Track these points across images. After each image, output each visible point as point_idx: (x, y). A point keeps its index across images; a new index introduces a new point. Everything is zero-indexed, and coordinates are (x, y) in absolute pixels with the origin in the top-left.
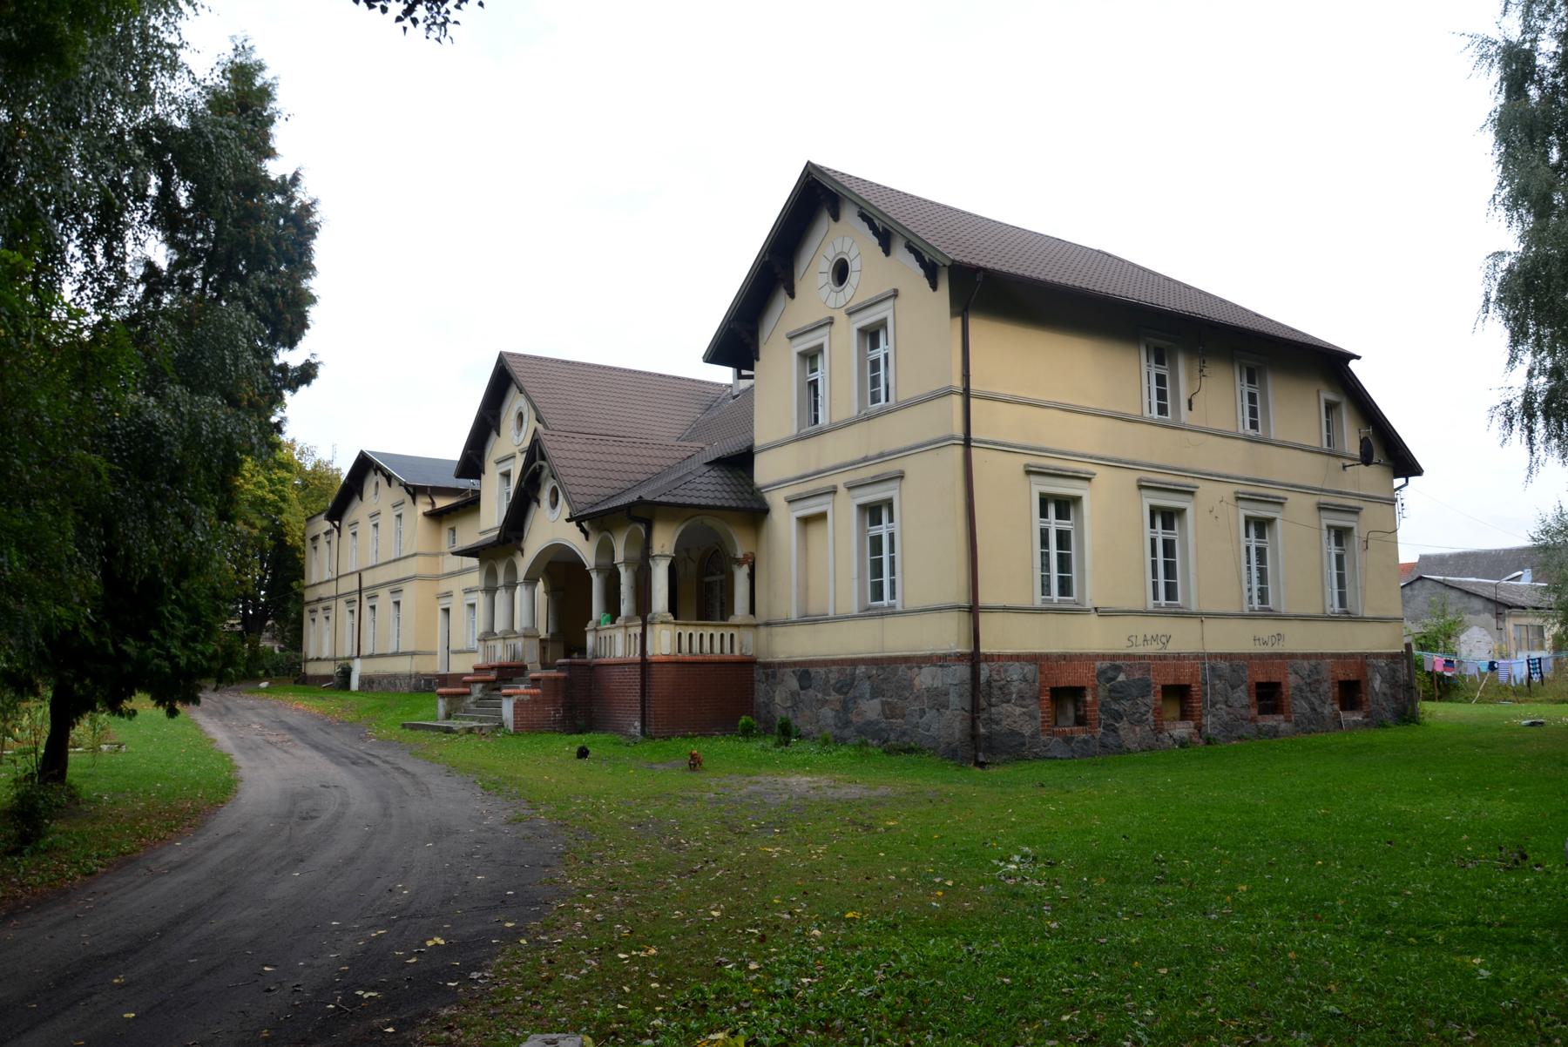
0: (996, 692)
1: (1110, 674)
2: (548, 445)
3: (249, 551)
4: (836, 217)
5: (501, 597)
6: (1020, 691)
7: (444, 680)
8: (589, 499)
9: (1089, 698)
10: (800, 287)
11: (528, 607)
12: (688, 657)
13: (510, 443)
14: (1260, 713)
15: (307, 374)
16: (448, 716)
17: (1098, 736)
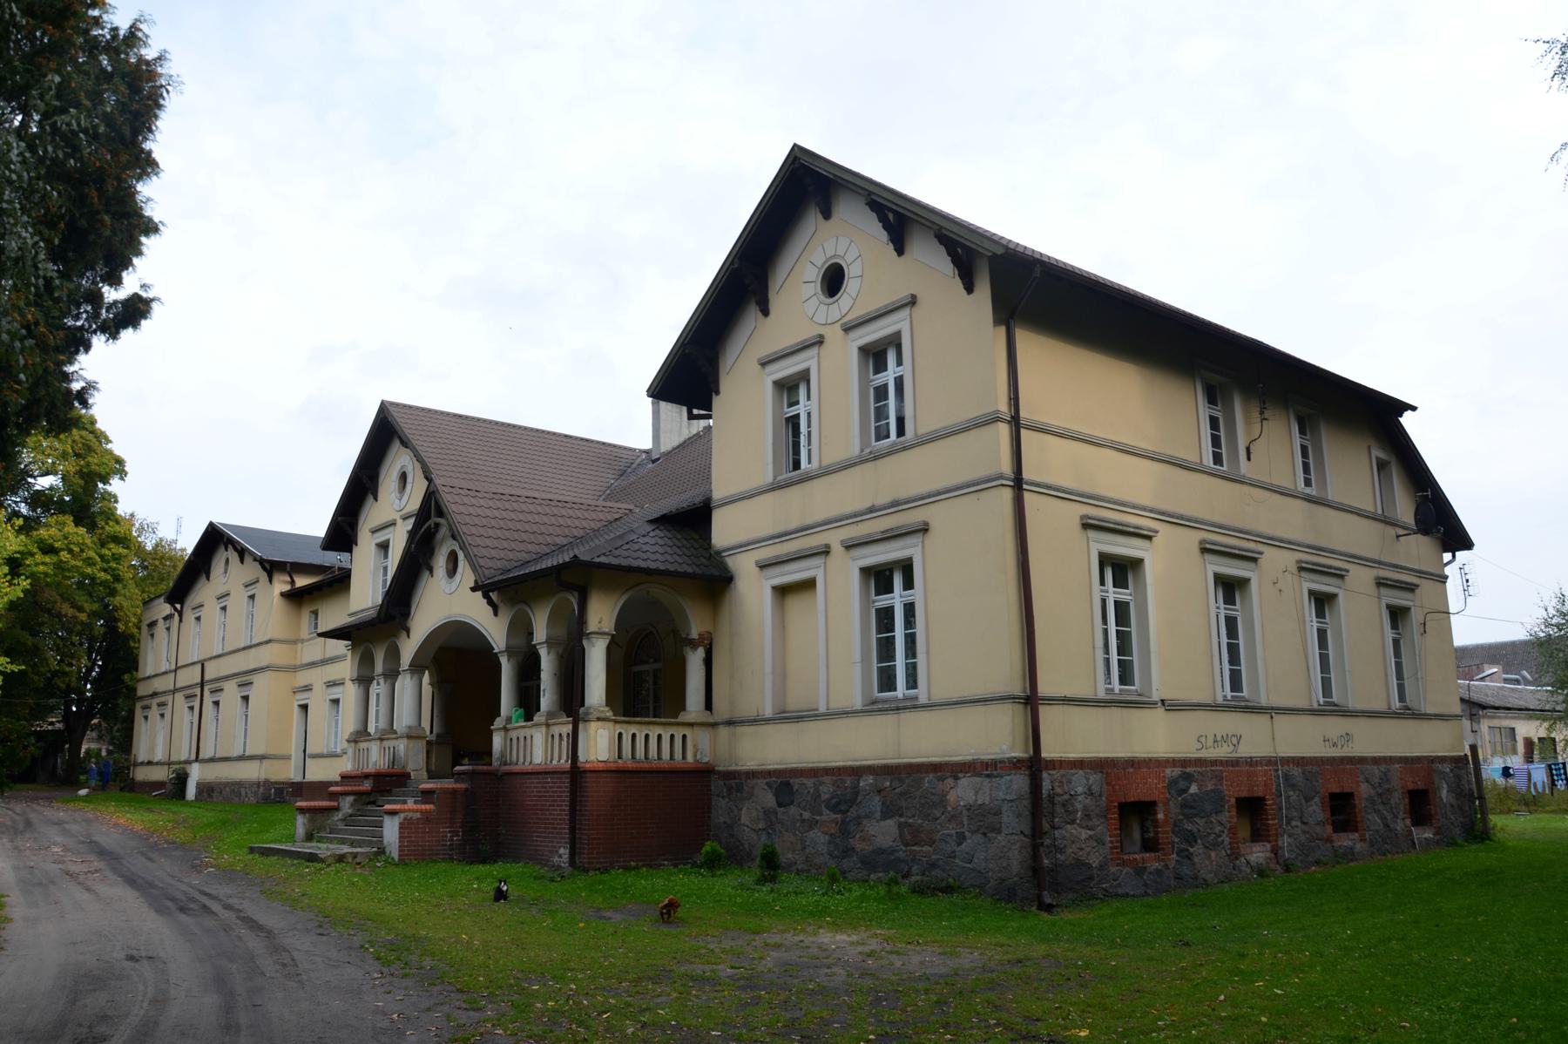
0: (1059, 809)
1: (1182, 784)
2: (447, 498)
3: (76, 639)
4: (827, 215)
5: (378, 689)
6: (1085, 809)
7: (300, 789)
8: (499, 564)
9: (1160, 816)
10: (777, 302)
11: (410, 701)
12: (630, 765)
13: (393, 508)
14: (1335, 831)
15: (135, 311)
16: (309, 837)
17: (1172, 864)
